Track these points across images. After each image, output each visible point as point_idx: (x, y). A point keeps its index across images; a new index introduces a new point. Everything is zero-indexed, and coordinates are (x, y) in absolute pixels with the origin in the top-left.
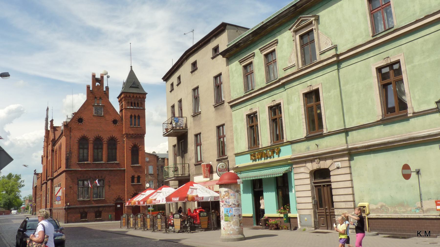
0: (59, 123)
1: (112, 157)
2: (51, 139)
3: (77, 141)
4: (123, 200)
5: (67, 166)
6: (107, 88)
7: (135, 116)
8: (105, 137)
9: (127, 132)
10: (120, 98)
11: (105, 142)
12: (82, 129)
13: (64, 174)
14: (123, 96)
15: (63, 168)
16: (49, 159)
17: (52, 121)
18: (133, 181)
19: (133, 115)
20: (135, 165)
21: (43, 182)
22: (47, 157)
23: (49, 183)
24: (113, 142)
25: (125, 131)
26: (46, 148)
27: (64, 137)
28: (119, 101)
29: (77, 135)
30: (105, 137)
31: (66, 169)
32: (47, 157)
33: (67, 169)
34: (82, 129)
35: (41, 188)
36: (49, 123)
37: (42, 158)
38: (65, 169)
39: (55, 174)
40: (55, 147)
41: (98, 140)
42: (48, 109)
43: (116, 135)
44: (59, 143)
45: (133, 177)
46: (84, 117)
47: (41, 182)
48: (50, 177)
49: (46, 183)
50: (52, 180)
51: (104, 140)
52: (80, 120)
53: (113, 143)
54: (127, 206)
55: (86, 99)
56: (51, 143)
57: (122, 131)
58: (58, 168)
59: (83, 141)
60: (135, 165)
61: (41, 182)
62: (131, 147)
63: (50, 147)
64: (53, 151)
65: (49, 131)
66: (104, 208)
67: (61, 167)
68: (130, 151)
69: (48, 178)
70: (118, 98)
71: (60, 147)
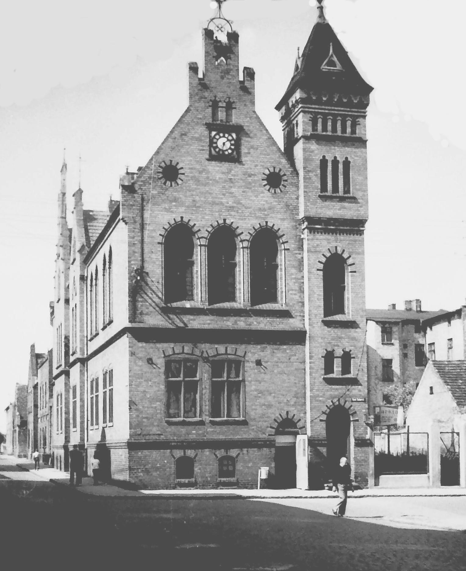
2: (78, 246)
3: (160, 239)
4: (300, 424)
5: (134, 313)
6: (250, 73)
7: (335, 162)
8: (246, 226)
10: (283, 109)
11: (246, 244)
12: (175, 200)
13: (125, 340)
14: (298, 95)
15: (122, 320)
16: (72, 304)
17: (79, 193)
18: (329, 369)
20: (182, 368)
21: (55, 372)
22: (67, 301)
24: (266, 242)
26: (62, 276)
27: (121, 224)
30: (246, 226)
32: (67, 301)
34: (175, 200)
35: (51, 390)
38: (128, 324)
39: (93, 346)
40: (92, 268)
41: (223, 238)
43: (280, 222)
44: (104, 250)
45: (329, 357)
48: (78, 355)
49: (67, 374)
50: (84, 361)
51: (243, 237)
52: (170, 173)
53: (266, 242)
56: (78, 256)
57: (296, 208)
58: (101, 326)
59: (178, 239)
60: (182, 368)
62: (324, 260)
63: (76, 271)
64: (83, 278)
65: (70, 230)
67: (111, 322)
69: (72, 359)
70: (278, 108)
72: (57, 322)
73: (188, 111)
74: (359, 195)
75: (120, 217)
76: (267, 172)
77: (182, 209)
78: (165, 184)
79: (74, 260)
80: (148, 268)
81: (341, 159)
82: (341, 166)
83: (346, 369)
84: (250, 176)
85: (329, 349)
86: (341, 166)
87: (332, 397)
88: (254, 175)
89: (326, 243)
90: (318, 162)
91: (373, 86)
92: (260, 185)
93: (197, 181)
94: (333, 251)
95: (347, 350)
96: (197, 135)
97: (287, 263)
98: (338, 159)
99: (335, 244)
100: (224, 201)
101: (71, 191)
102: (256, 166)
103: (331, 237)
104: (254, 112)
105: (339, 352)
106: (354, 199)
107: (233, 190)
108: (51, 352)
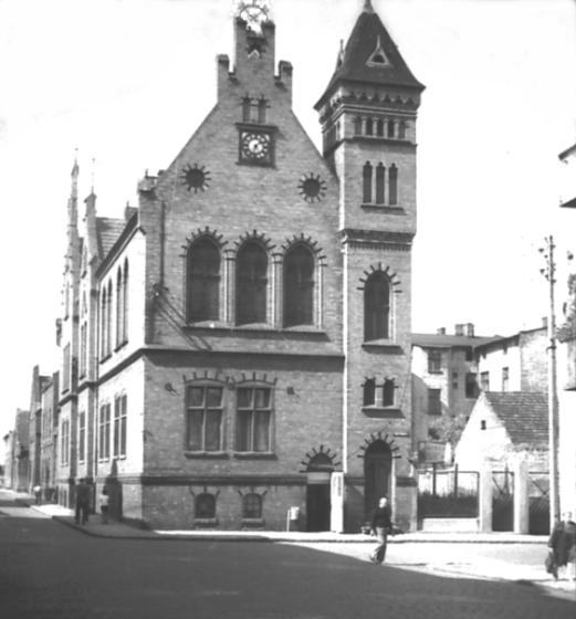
0: (116, 203)
1: (297, 307)
2: (90, 257)
4: (335, 461)
5: (151, 332)
6: (286, 68)
7: (381, 168)
9: (353, 226)
10: (323, 110)
13: (140, 365)
14: (340, 93)
15: (137, 340)
16: (82, 322)
17: (91, 200)
18: (368, 398)
19: (374, 164)
21: (61, 397)
22: (76, 319)
23: (84, 397)
24: (300, 257)
25: (346, 223)
27: (139, 235)
28: (322, 120)
29: (183, 228)
30: (279, 238)
31: (146, 347)
32: (76, 319)
33: (152, 347)
36: (82, 208)
37: (59, 325)
40: (105, 282)
41: (253, 251)
42: (76, 170)
43: (317, 234)
44: (120, 262)
45: (369, 386)
46: (211, 167)
47: (56, 396)
48: (87, 379)
49: (74, 399)
50: (93, 386)
54: (291, 521)
55: (212, 101)
56: (89, 269)
57: (336, 219)
58: (114, 347)
59: (203, 250)
61: (56, 396)
62: (365, 277)
63: (86, 285)
64: (94, 293)
66: (273, 488)
67: (125, 343)
68: (362, 292)
69: (80, 383)
70: (317, 107)
71: (123, 275)
72: (64, 342)
73: (216, 109)
74: (406, 206)
75: (138, 226)
76: (303, 179)
77: (207, 219)
78: (189, 189)
79: (85, 273)
80: (169, 283)
81: (387, 165)
82: (387, 173)
83: (388, 399)
84: (285, 182)
85: (370, 377)
86: (387, 173)
87: (371, 431)
88: (290, 182)
89: (368, 259)
90: (361, 169)
91: (424, 84)
92: (296, 194)
93: (225, 187)
94: (376, 268)
95: (390, 378)
96: (226, 136)
97: (325, 280)
98: (384, 165)
99: (377, 260)
100: (255, 209)
101: (82, 195)
102: (292, 171)
103: (373, 252)
104: (291, 111)
105: (380, 381)
106: (400, 211)
107: (265, 198)
108: (56, 375)
